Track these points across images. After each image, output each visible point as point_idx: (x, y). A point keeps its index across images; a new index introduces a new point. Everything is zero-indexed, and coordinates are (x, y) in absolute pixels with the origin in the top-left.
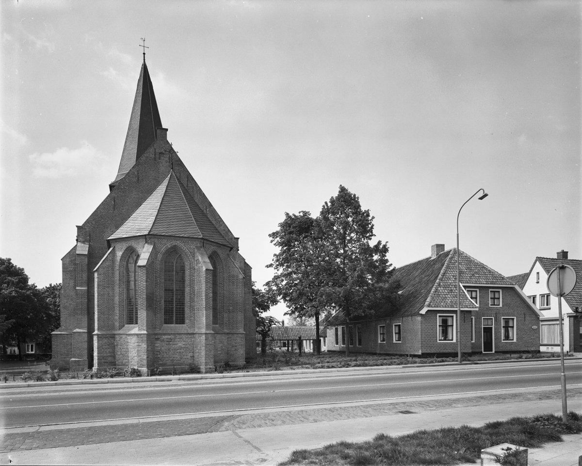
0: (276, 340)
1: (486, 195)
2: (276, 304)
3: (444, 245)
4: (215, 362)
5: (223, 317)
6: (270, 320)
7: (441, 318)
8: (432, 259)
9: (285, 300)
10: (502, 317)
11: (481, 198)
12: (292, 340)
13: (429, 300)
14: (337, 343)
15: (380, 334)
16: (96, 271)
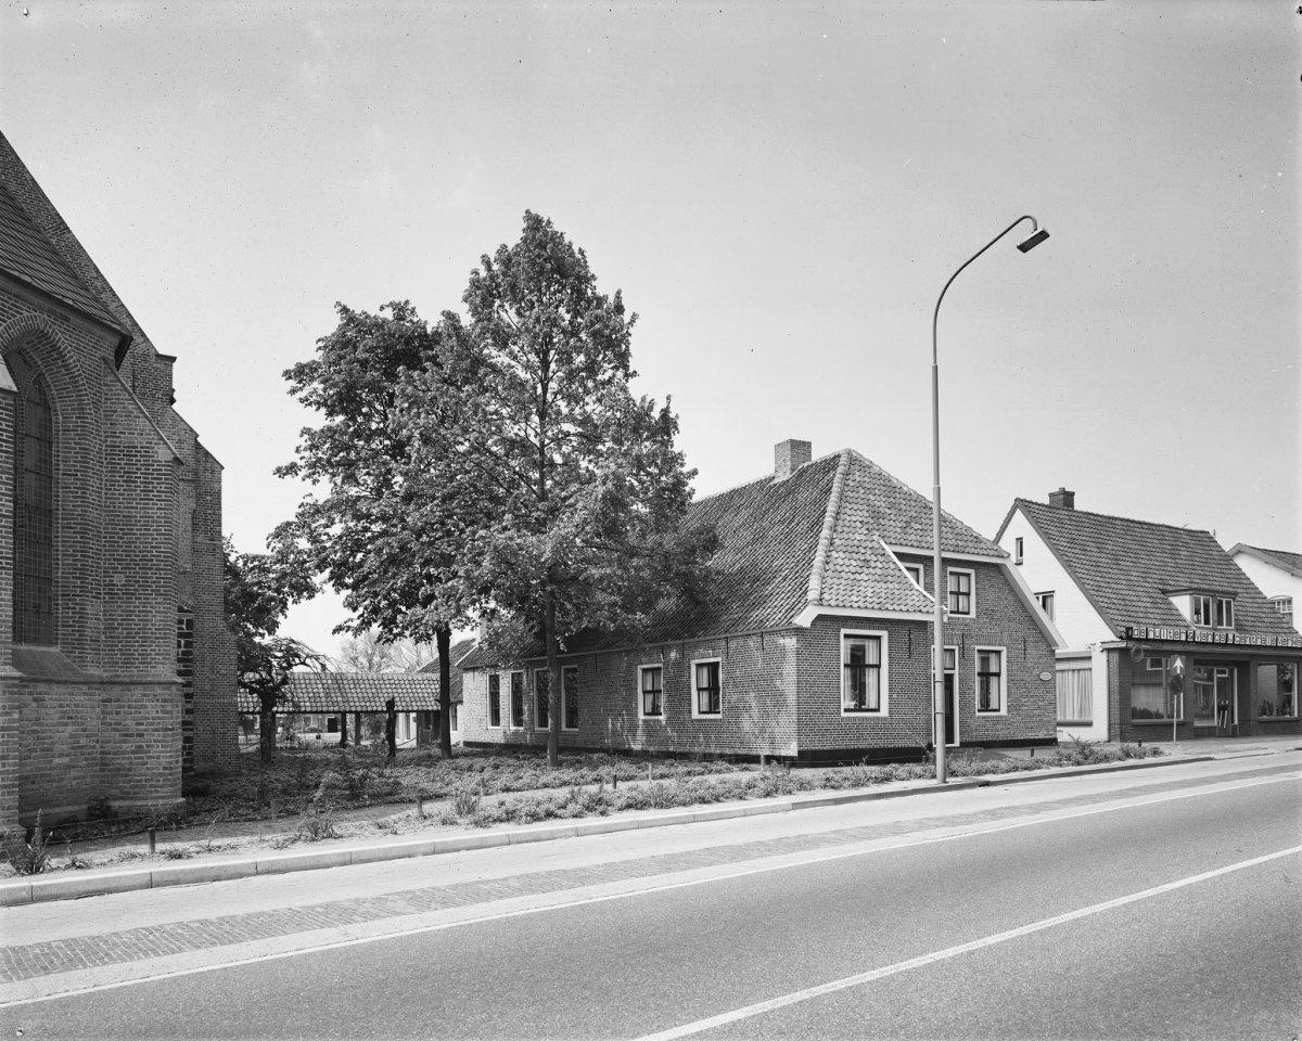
0: (305, 712)
1: (1043, 236)
2: (310, 597)
3: (809, 445)
4: (26, 804)
5: (82, 615)
6: (289, 649)
7: (851, 642)
8: (776, 481)
9: (339, 584)
10: (977, 647)
11: (1024, 248)
12: (358, 714)
13: (814, 583)
14: (496, 720)
15: (645, 692)
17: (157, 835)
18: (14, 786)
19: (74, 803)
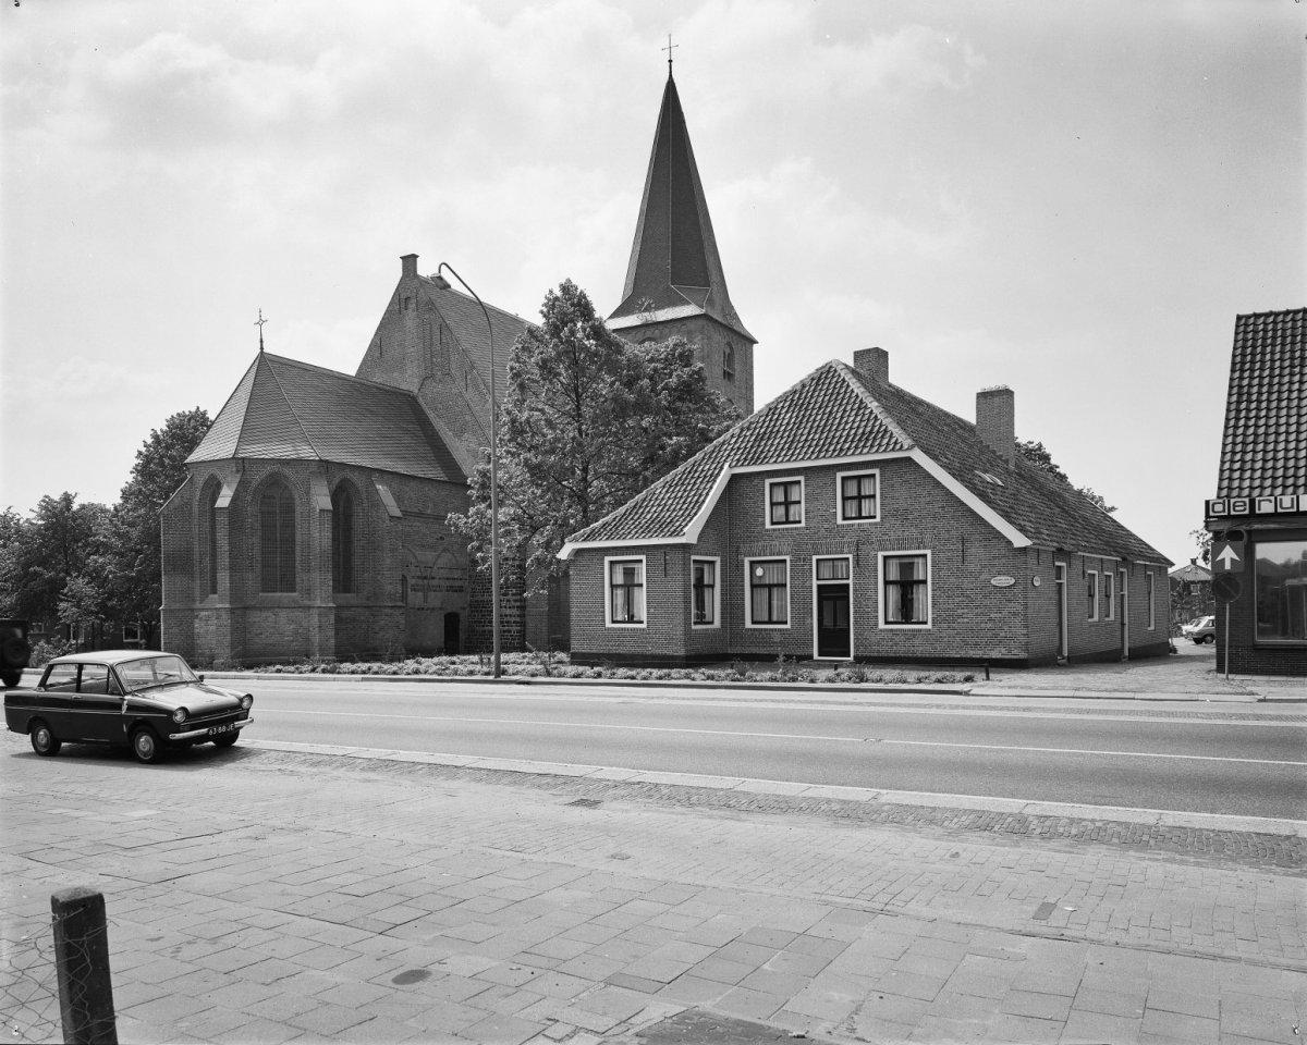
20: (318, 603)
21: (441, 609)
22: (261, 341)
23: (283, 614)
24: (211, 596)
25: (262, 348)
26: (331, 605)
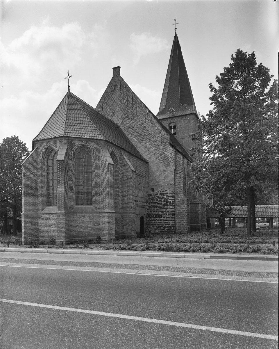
16: (23, 165)
17: (9, 245)
18: (64, 233)
19: (94, 237)
20: (107, 210)
21: (139, 215)
22: (69, 86)
23: (87, 216)
24: (47, 207)
25: (69, 90)
26: (113, 212)
